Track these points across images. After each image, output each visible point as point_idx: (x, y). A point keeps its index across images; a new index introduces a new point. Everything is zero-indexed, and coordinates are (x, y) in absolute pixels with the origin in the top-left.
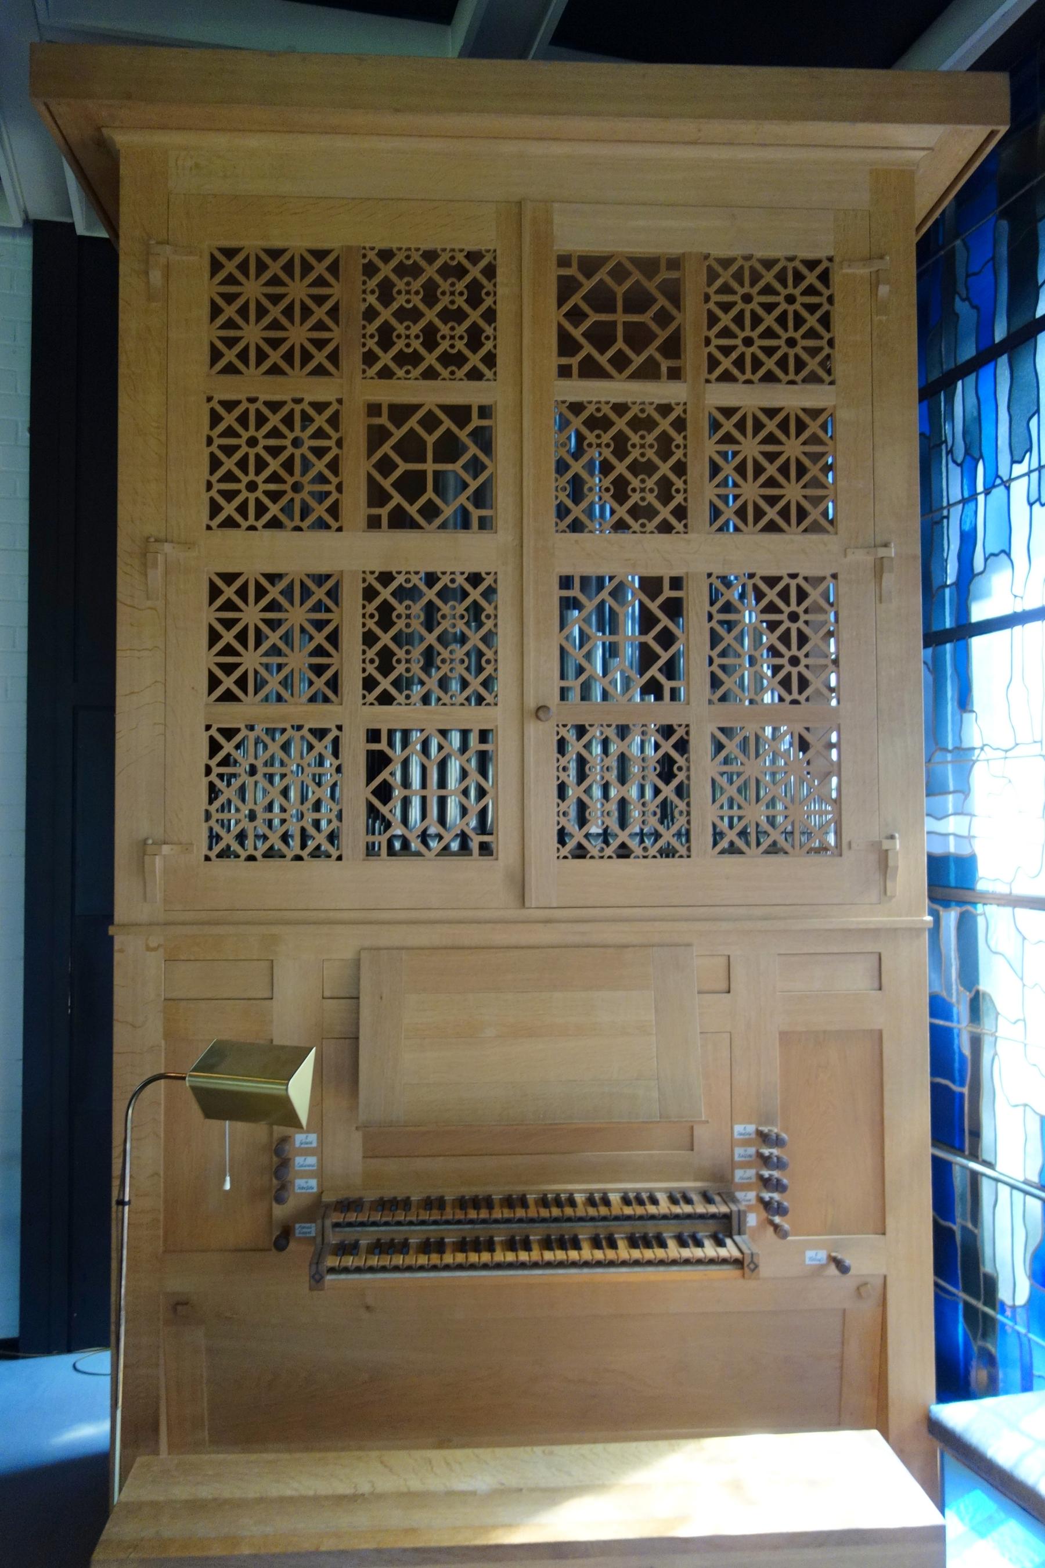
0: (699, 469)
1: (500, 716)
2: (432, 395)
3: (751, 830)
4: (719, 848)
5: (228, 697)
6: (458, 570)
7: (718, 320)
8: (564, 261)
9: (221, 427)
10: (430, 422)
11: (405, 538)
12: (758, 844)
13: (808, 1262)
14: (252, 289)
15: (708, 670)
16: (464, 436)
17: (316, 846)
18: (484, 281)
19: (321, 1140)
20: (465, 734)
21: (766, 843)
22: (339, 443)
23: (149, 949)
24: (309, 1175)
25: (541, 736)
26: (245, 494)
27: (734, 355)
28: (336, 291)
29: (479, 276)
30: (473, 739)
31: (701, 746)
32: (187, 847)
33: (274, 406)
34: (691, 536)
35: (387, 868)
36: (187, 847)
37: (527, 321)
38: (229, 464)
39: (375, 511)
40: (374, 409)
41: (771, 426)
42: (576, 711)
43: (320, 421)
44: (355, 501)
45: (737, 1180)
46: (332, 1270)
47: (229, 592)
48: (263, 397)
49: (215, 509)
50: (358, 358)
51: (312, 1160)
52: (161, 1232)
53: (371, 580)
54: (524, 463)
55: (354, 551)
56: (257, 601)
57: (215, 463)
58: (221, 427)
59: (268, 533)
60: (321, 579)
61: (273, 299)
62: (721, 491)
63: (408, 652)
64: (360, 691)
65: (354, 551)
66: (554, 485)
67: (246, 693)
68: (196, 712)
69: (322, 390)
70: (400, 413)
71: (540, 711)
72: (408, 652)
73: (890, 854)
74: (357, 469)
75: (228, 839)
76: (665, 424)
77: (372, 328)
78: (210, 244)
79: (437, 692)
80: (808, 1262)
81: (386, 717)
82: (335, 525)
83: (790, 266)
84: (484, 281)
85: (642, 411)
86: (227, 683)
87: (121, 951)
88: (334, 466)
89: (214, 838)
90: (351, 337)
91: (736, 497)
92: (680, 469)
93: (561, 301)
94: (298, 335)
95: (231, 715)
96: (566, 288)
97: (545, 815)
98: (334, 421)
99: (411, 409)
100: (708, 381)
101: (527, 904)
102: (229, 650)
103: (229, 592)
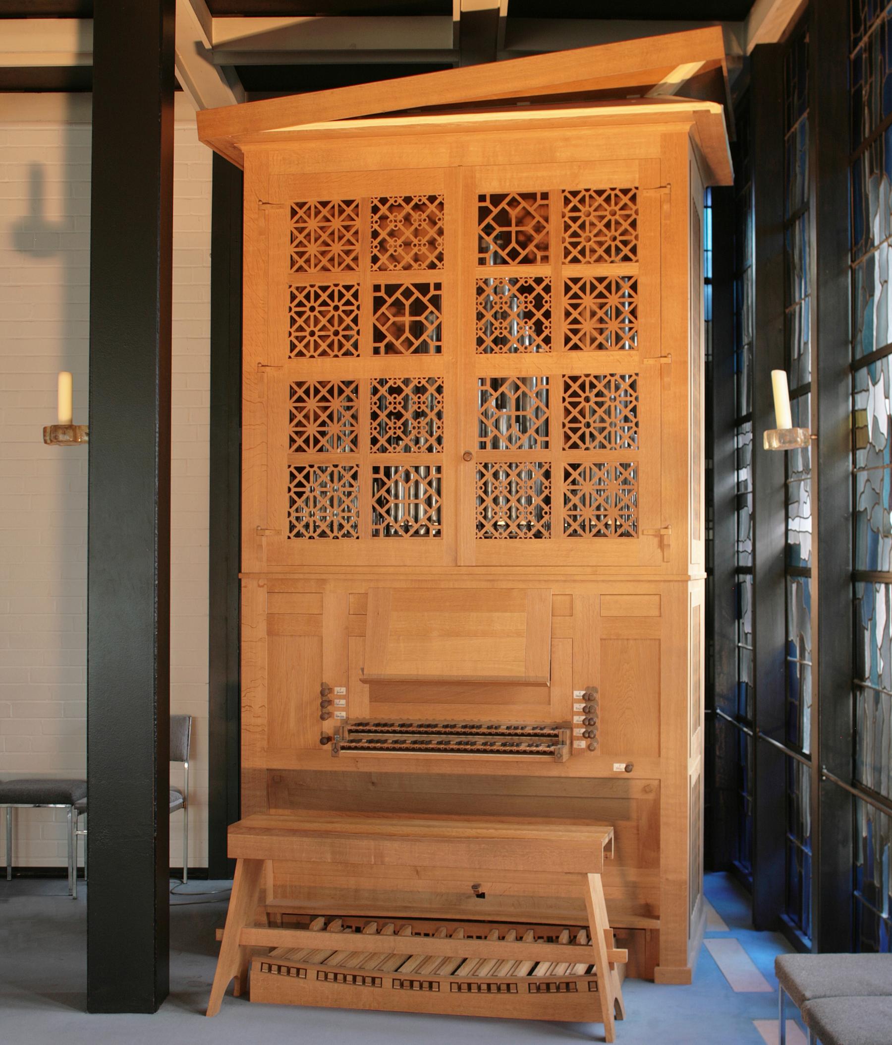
0: (558, 315)
1: (445, 457)
2: (407, 279)
3: (587, 523)
4: (568, 533)
5: (300, 449)
6: (422, 377)
7: (570, 227)
8: (482, 198)
9: (296, 302)
10: (407, 293)
11: (392, 359)
12: (590, 531)
13: (615, 770)
14: (313, 224)
15: (562, 431)
16: (425, 300)
17: (343, 531)
18: (388, 385)
19: (348, 691)
20: (428, 469)
21: (594, 531)
22: (358, 308)
23: (259, 586)
24: (342, 709)
25: (470, 470)
26: (308, 338)
27: (579, 248)
28: (358, 224)
29: (435, 210)
30: (433, 471)
31: (558, 475)
32: (278, 532)
33: (324, 289)
34: (554, 354)
35: (382, 542)
36: (278, 532)
37: (461, 230)
38: (300, 322)
39: (377, 345)
40: (377, 288)
41: (601, 288)
42: (489, 455)
43: (348, 296)
44: (366, 340)
45: (575, 722)
46: (343, 748)
47: (300, 392)
48: (318, 284)
49: (293, 347)
50: (369, 259)
51: (343, 702)
52: (266, 737)
53: (375, 383)
54: (457, 316)
55: (365, 367)
56: (315, 396)
57: (293, 321)
58: (296, 302)
59: (320, 359)
60: (348, 383)
61: (322, 222)
62: (622, 300)
63: (526, 307)
64: (445, 385)
65: (365, 367)
66: (475, 327)
67: (309, 447)
68: (283, 458)
69: (348, 279)
70: (391, 289)
71: (467, 456)
72: (526, 307)
73: (665, 537)
74: (367, 320)
75: (300, 527)
76: (539, 289)
77: (376, 243)
78: (290, 203)
79: (435, 445)
80: (615, 770)
81: (383, 459)
82: (356, 353)
83: (568, 240)
84: (388, 385)
85: (526, 282)
86: (300, 442)
87: (245, 587)
88: (355, 321)
89: (292, 527)
90: (364, 248)
91: (630, 304)
92: (547, 315)
93: (481, 221)
94: (337, 248)
95: (302, 460)
96: (483, 213)
97: (470, 513)
98: (355, 296)
99: (398, 287)
100: (563, 263)
101: (542, 673)
102: (299, 424)
103: (300, 392)
